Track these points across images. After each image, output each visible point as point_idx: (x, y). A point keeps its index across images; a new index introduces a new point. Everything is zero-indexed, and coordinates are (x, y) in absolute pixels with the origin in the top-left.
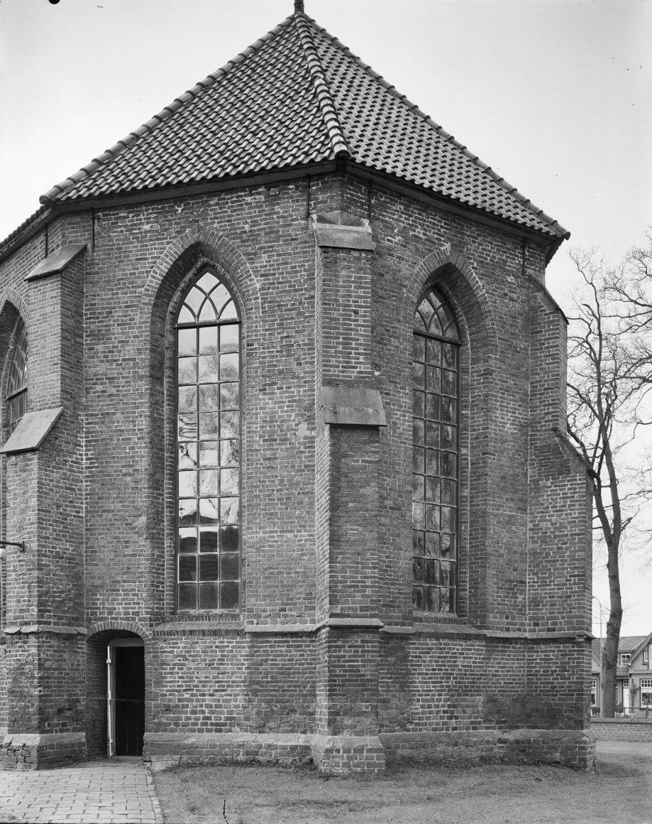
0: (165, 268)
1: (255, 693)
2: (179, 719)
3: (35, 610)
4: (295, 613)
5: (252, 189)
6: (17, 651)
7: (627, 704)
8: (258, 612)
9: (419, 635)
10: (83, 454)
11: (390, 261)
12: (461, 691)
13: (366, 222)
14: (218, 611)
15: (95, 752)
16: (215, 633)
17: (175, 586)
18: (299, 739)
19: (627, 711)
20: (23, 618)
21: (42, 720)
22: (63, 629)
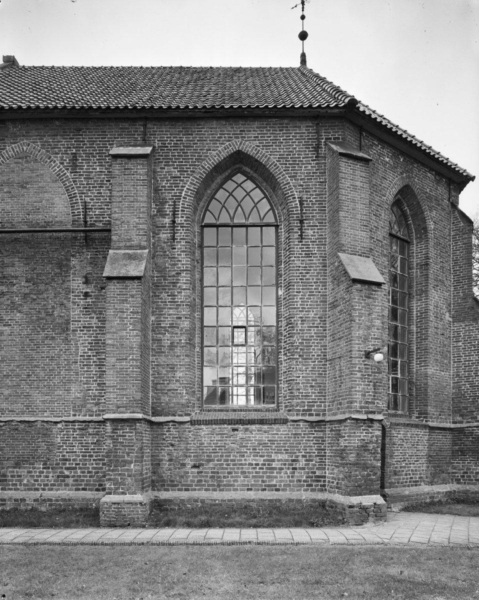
2: (400, 479)
4: (444, 417)
6: (362, 433)
20: (368, 408)
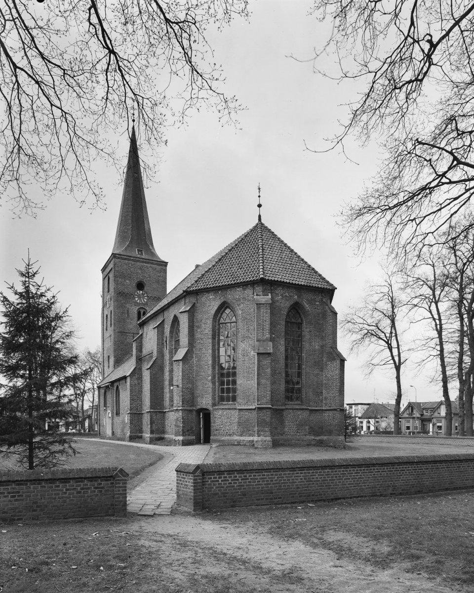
0: (216, 308)
1: (240, 425)
3: (181, 403)
5: (239, 287)
7: (431, 430)
8: (241, 404)
9: (287, 409)
10: (195, 360)
11: (277, 304)
12: (300, 425)
13: (270, 294)
14: (231, 403)
15: (197, 442)
16: (229, 409)
17: (219, 396)
18: (251, 438)
19: (431, 433)
21: (183, 433)
22: (189, 408)
